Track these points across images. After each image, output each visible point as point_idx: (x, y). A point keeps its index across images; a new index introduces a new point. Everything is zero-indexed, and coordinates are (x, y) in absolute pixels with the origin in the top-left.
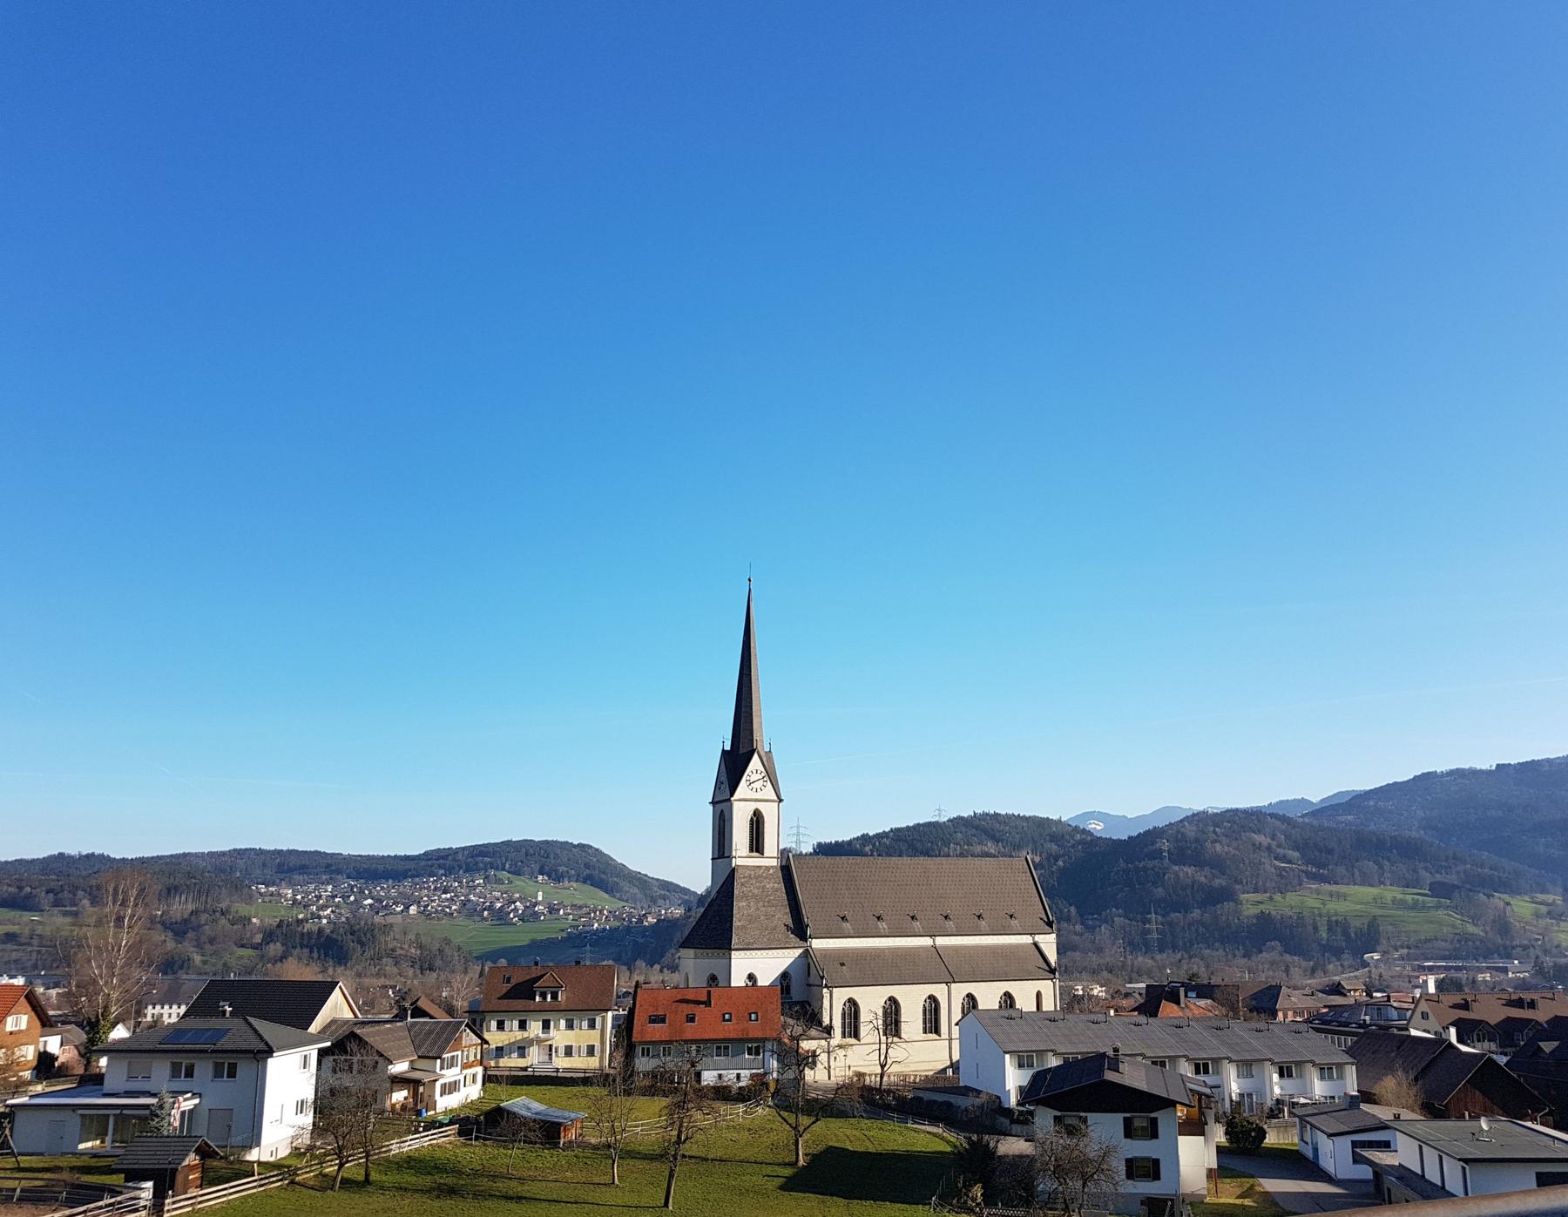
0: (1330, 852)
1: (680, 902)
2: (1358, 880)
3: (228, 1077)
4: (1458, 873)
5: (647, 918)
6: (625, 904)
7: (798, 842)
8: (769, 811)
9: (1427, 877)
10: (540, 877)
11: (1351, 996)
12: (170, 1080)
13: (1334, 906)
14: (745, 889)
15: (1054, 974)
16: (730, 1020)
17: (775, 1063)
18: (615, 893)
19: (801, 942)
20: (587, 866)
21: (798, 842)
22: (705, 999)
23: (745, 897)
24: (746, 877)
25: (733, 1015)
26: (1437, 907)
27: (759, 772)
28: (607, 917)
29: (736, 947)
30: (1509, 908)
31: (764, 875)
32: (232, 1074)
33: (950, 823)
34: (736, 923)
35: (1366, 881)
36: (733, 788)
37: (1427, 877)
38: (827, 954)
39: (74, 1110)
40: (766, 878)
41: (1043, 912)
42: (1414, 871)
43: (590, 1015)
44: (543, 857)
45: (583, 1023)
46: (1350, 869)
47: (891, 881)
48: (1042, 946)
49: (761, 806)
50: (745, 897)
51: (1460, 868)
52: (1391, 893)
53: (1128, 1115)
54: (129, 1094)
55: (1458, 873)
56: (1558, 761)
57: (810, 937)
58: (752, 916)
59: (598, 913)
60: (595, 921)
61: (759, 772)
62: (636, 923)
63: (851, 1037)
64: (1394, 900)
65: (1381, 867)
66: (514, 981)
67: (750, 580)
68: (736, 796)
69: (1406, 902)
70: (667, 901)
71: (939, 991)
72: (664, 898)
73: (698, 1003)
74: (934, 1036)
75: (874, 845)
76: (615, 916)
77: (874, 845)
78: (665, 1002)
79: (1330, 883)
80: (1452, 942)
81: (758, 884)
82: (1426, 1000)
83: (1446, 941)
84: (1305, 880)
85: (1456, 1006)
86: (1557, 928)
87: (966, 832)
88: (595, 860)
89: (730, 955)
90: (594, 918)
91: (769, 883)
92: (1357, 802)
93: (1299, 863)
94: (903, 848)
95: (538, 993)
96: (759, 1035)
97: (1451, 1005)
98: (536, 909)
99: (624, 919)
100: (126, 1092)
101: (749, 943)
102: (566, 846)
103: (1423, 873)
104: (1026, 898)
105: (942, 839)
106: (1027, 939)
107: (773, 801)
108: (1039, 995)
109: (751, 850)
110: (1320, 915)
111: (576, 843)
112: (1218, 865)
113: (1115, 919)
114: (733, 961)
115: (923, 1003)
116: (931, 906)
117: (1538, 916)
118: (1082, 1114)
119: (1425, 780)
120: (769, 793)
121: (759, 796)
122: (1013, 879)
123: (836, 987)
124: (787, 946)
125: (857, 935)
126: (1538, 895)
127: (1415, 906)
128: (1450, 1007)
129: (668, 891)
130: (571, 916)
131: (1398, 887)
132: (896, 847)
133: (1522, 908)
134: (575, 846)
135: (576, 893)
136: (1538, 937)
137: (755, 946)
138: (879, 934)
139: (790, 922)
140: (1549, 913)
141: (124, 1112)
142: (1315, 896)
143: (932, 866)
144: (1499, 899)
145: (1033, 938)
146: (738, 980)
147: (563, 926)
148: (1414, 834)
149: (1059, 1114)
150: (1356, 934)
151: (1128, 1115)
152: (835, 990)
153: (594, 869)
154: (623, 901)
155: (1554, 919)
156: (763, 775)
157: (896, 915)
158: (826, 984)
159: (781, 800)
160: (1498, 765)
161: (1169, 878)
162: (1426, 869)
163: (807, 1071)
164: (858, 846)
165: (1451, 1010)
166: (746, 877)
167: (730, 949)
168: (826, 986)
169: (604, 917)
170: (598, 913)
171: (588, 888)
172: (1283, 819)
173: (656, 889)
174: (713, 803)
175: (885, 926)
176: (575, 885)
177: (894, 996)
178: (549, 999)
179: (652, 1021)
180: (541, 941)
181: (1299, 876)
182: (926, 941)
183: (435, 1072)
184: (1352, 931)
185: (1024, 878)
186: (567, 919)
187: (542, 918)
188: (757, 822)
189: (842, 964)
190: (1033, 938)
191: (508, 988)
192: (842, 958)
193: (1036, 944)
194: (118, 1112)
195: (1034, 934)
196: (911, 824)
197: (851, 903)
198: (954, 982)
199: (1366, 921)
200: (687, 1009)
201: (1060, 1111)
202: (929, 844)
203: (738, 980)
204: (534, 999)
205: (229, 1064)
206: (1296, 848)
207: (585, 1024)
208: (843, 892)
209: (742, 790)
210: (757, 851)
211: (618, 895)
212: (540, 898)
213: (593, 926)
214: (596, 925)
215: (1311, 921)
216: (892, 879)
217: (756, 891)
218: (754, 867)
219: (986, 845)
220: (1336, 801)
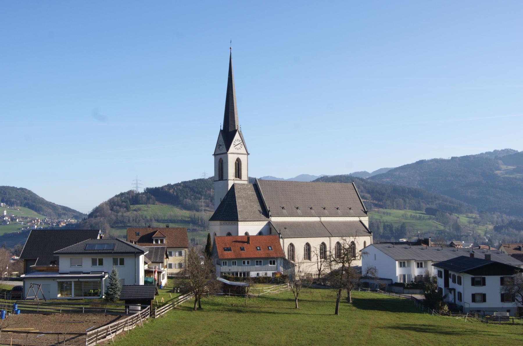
0: (383, 194)
1: (72, 216)
2: (395, 206)
3: (120, 265)
4: (436, 204)
5: (61, 223)
6: (45, 217)
7: (137, 187)
8: (243, 159)
9: (424, 206)
10: (2, 204)
12: (92, 267)
14: (240, 194)
15: (371, 234)
16: (260, 250)
17: (282, 269)
18: (40, 212)
19: (267, 218)
20: (25, 198)
21: (137, 187)
22: (247, 241)
23: (240, 198)
24: (239, 189)
25: (261, 248)
26: (429, 219)
27: (239, 140)
28: (40, 223)
29: (240, 220)
30: (458, 219)
31: (247, 188)
32: (122, 263)
33: (210, 180)
34: (239, 210)
35: (398, 207)
36: (228, 147)
37: (424, 206)
39: (54, 280)
40: (247, 189)
41: (362, 207)
42: (419, 203)
43: (179, 250)
44: (3, 194)
45: (176, 253)
47: (300, 192)
48: (363, 222)
49: (240, 157)
50: (240, 198)
51: (437, 202)
52: (410, 213)
53: (502, 276)
54: (71, 273)
55: (436, 204)
56: (476, 156)
57: (271, 216)
58: (244, 206)
59: (36, 221)
60: (35, 225)
61: (239, 140)
62: (56, 226)
63: (307, 259)
64: (411, 216)
65: (405, 201)
66: (141, 235)
67: (231, 48)
69: (416, 216)
70: (66, 216)
71: (326, 240)
72: (65, 214)
73: (244, 242)
74: (308, 261)
75: (174, 189)
76: (45, 223)
77: (174, 189)
78: (228, 242)
79: (383, 208)
80: (436, 234)
81: (245, 192)
82: (504, 247)
83: (433, 233)
84: (373, 207)
85: (516, 249)
86: (478, 228)
88: (29, 196)
89: (238, 223)
90: (34, 223)
91: (249, 192)
92: (391, 172)
93: (370, 199)
94: (188, 191)
95: (154, 240)
96: (275, 256)
97: (514, 248)
98: (5, 219)
99: (49, 224)
100: (70, 272)
101: (245, 218)
102: (13, 189)
103: (422, 204)
104: (355, 201)
105: (207, 187)
106: (356, 219)
107: (246, 155)
109: (236, 177)
110: (380, 222)
111: (18, 187)
114: (239, 226)
115: (304, 246)
116: (318, 204)
117: (470, 223)
118: (483, 276)
119: (421, 163)
120: (243, 151)
121: (239, 151)
122: (348, 192)
123: (285, 238)
124: (261, 220)
125: (289, 216)
126: (469, 214)
127: (420, 218)
128: (514, 249)
129: (66, 211)
130: (23, 222)
131: (412, 210)
132: (185, 190)
133: (463, 219)
134: (18, 189)
135: (20, 212)
136: (470, 232)
137: (248, 220)
138: (298, 215)
139: (260, 209)
140: (474, 222)
141: (80, 280)
142: (377, 214)
143: (315, 186)
144: (455, 216)
145: (360, 218)
146: (241, 233)
147: (19, 227)
148: (415, 187)
149: (473, 276)
150: (395, 230)
151: (502, 276)
152: (285, 239)
153: (29, 200)
154: (44, 215)
155: (476, 224)
156: (241, 142)
157: (304, 207)
158: (281, 237)
159: (248, 154)
160: (452, 157)
162: (423, 202)
165: (514, 250)
166: (239, 189)
168: (282, 238)
169: (39, 223)
170: (36, 221)
171: (26, 209)
172: (362, 180)
173: (60, 210)
174: (215, 155)
175: (300, 212)
176: (20, 207)
177: (293, 243)
178: (159, 243)
179: (225, 250)
180: (9, 234)
181: (370, 205)
182: (317, 219)
183: (160, 269)
184: (394, 229)
185: (353, 192)
186: (21, 224)
187: (8, 223)
188: (238, 163)
189: (285, 228)
190: (360, 218)
191: (139, 238)
192: (285, 226)
193: (360, 221)
194: (77, 280)
195: (360, 217)
196: (191, 180)
197: (285, 201)
198: (332, 237)
199: (400, 225)
200: (240, 245)
201: (474, 275)
202: (201, 189)
203: (241, 233)
204: (153, 243)
205: (99, 259)
206: (369, 192)
207: (177, 254)
208: (281, 196)
209: (232, 149)
210: (238, 177)
211: (42, 213)
212: (5, 214)
213: (35, 227)
214: (36, 227)
215: (376, 225)
216: (300, 191)
217: (244, 195)
218: (241, 184)
220: (381, 173)
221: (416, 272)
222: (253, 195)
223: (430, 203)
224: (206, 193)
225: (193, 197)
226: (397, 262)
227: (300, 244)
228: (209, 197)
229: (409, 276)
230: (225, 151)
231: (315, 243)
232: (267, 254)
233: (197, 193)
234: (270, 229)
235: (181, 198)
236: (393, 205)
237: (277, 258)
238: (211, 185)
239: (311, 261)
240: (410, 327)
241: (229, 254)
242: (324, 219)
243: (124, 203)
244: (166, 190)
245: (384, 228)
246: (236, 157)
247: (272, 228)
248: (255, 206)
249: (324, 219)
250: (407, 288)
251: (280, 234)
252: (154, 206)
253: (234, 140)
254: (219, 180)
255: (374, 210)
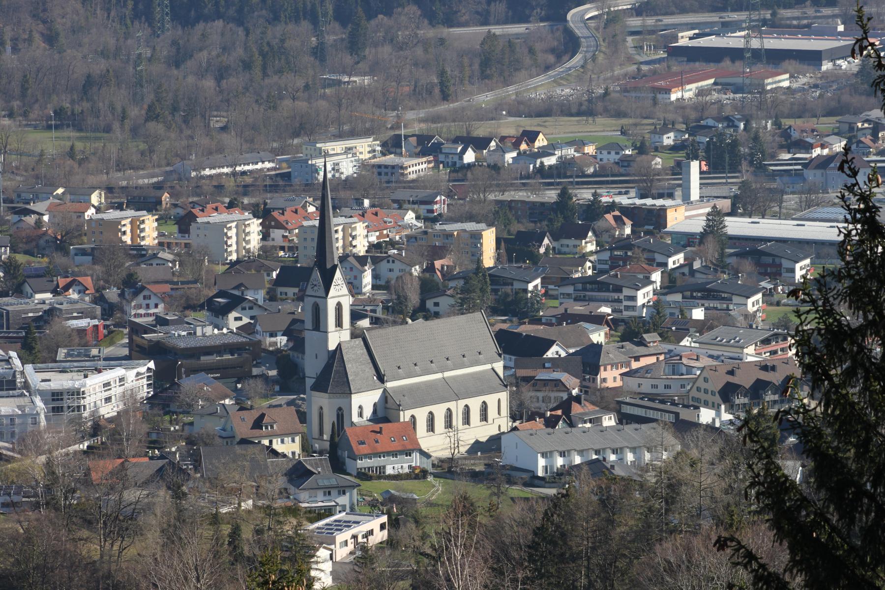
11: (651, 347)
16: (394, 441)
68: (329, 296)
101: (359, 389)
106: (488, 367)
108: (499, 401)
121: (340, 293)
163: (144, 390)
167: (351, 393)
179: (359, 444)
182: (439, 376)
193: (493, 369)
217: (353, 356)
221: (560, 462)
222: (362, 354)
226: (539, 455)
227: (421, 414)
229: (552, 467)
230: (322, 293)
232: (403, 445)
234: (386, 398)
237: (413, 450)
239: (342, 327)
240: (776, 88)
242: (447, 374)
246: (336, 301)
247: (389, 397)
248: (367, 370)
249: (447, 374)
250: (549, 482)
251: (399, 405)
253: (334, 280)
254: (313, 330)
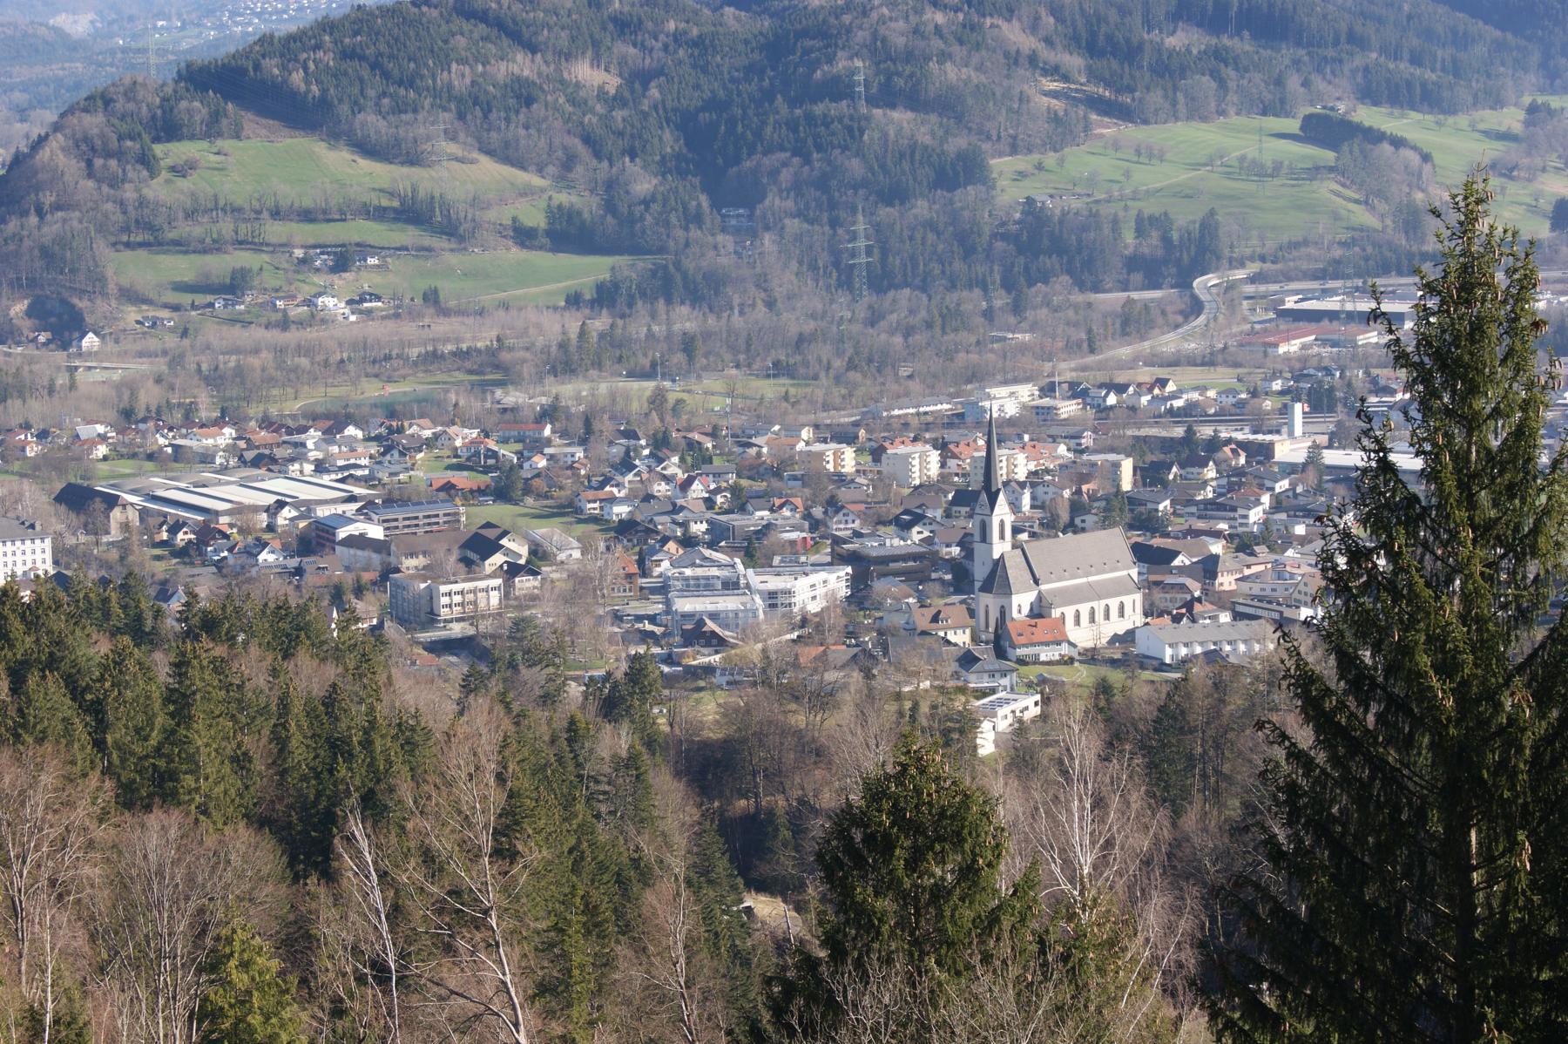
13: (1149, 177)
35: (1196, 113)
38: (1048, 591)
46: (1170, 93)
87: (471, 32)
106: (1125, 573)
112: (949, 106)
113: (787, 221)
161: (871, 139)
164: (276, 71)
182: (1084, 580)
192: (1055, 592)
202: (412, 65)
206: (1075, 42)
209: (997, 510)
219: (514, 61)
221: (1183, 651)
223: (1328, 70)
224: (434, 80)
225: (386, 101)
227: (1069, 612)
228: (449, 101)
231: (1084, 609)
233: (400, 83)
235: (344, 109)
236: (1174, 104)
238: (446, 42)
241: (1022, 640)
242: (1091, 579)
243: (129, 143)
244: (276, 71)
245: (1140, 232)
249: (1091, 579)
252: (241, 144)
255: (1102, 136)
